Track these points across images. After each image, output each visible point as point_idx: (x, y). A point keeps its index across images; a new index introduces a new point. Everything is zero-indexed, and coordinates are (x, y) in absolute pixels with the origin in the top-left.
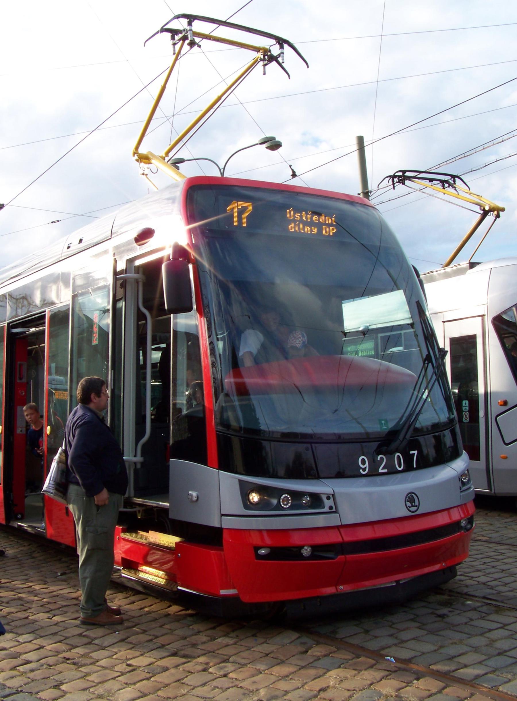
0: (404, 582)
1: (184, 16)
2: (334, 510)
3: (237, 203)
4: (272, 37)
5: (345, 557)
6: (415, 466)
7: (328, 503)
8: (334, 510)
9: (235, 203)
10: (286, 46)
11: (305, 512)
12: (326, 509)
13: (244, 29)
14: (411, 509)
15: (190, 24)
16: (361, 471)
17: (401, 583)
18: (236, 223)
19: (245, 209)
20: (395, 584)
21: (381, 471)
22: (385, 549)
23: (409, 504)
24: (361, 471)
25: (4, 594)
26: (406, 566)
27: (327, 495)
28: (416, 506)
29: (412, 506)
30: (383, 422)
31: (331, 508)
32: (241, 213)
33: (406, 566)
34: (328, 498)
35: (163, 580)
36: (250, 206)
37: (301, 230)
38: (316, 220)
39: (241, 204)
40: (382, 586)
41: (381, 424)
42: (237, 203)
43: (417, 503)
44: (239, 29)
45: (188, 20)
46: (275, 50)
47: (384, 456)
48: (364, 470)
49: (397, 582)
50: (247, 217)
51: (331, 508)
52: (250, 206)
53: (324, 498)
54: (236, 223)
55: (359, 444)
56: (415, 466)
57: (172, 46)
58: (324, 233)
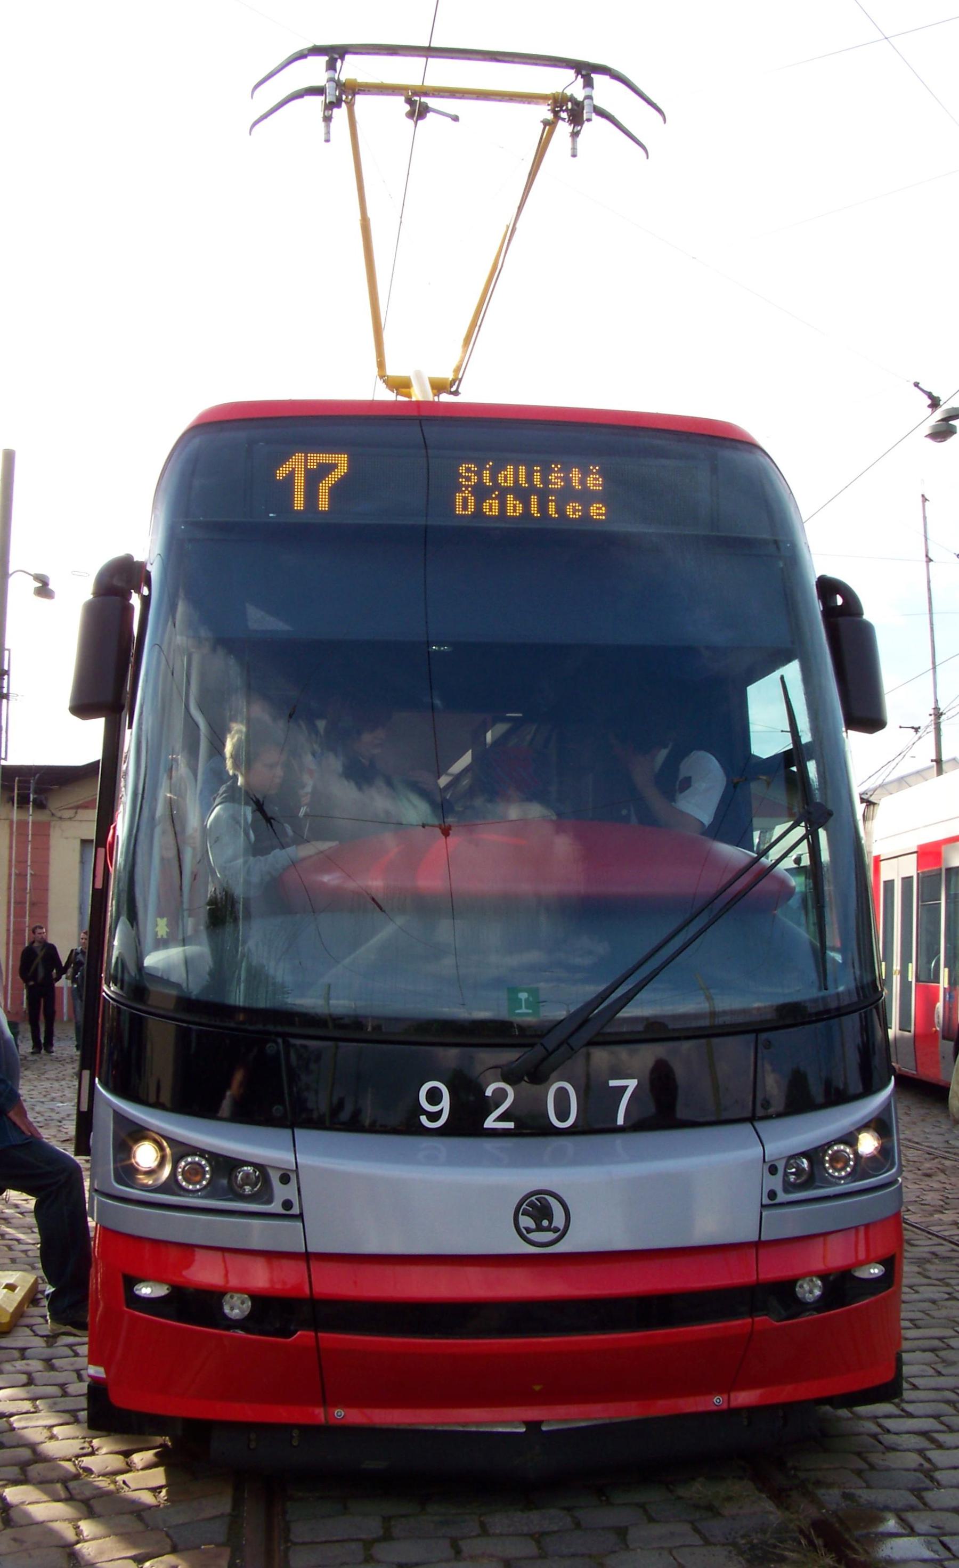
0: (558, 1430)
1: (317, 51)
2: (296, 1210)
3: (306, 457)
4: (560, 64)
5: (317, 1336)
6: (620, 1121)
7: (281, 1192)
8: (296, 1210)
9: (299, 456)
10: (597, 78)
11: (230, 1208)
12: (275, 1207)
13: (480, 57)
14: (534, 1236)
15: (331, 66)
16: (423, 1119)
17: (544, 1428)
18: (299, 503)
19: (326, 469)
20: (523, 1430)
21: (490, 1123)
22: (447, 1332)
23: (526, 1222)
24: (423, 1119)
25: (956, 1238)
26: (537, 1388)
27: (281, 1172)
28: (556, 1230)
29: (540, 1228)
30: (523, 996)
31: (287, 1204)
32: (314, 477)
33: (537, 1388)
34: (285, 1179)
35: (756, 1277)
36: (342, 462)
37: (534, 510)
38: (595, 485)
39: (316, 459)
40: (440, 1428)
41: (516, 1002)
42: (306, 457)
43: (559, 1220)
44: (536, 64)
45: (593, 75)
46: (577, 91)
47: (510, 1084)
48: (434, 1117)
49: (533, 1426)
50: (333, 490)
51: (287, 1204)
52: (342, 462)
53: (275, 1177)
54: (299, 503)
55: (703, 1041)
56: (620, 1121)
57: (570, 139)
58: (459, 511)
